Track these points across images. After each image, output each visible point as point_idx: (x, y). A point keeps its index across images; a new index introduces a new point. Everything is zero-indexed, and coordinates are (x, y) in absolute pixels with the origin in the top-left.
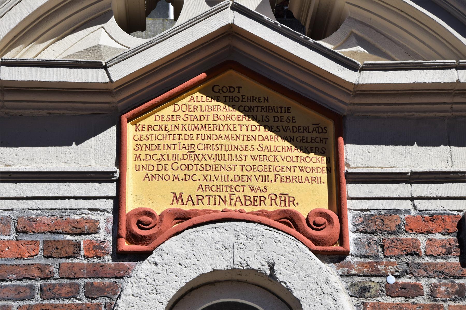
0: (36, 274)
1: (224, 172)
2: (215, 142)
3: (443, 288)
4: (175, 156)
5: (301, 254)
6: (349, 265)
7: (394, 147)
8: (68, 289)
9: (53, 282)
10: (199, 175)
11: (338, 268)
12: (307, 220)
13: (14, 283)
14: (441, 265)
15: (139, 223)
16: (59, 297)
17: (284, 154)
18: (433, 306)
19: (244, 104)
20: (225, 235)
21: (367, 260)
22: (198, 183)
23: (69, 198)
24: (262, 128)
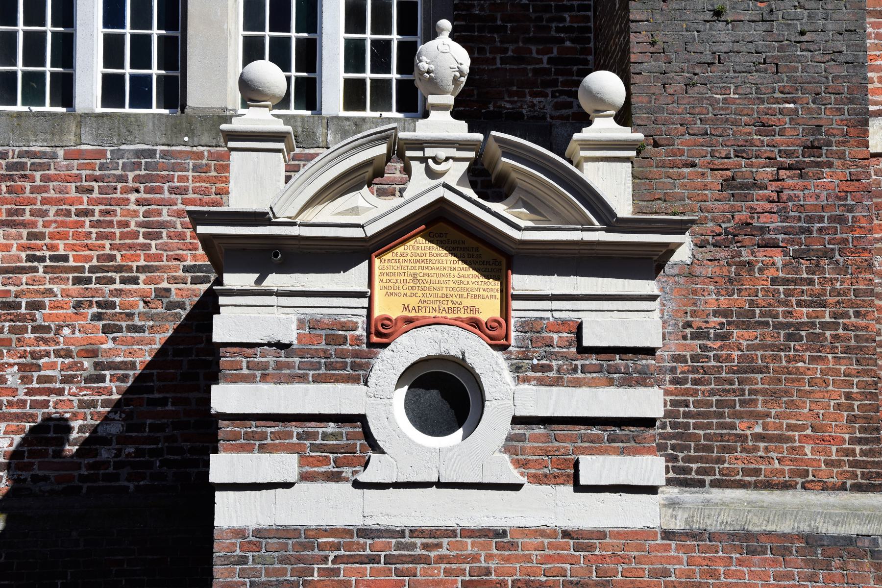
0: (322, 355)
1: (435, 292)
2: (430, 272)
3: (565, 367)
4: (405, 281)
5: (481, 346)
6: (511, 352)
7: (542, 277)
8: (341, 365)
9: (332, 360)
10: (420, 293)
11: (504, 354)
12: (486, 323)
13: (309, 360)
14: (565, 352)
15: (383, 325)
16: (336, 369)
17: (473, 280)
18: (558, 378)
19: (449, 245)
20: (436, 333)
21: (522, 349)
22: (419, 298)
23: (340, 307)
24: (460, 262)
